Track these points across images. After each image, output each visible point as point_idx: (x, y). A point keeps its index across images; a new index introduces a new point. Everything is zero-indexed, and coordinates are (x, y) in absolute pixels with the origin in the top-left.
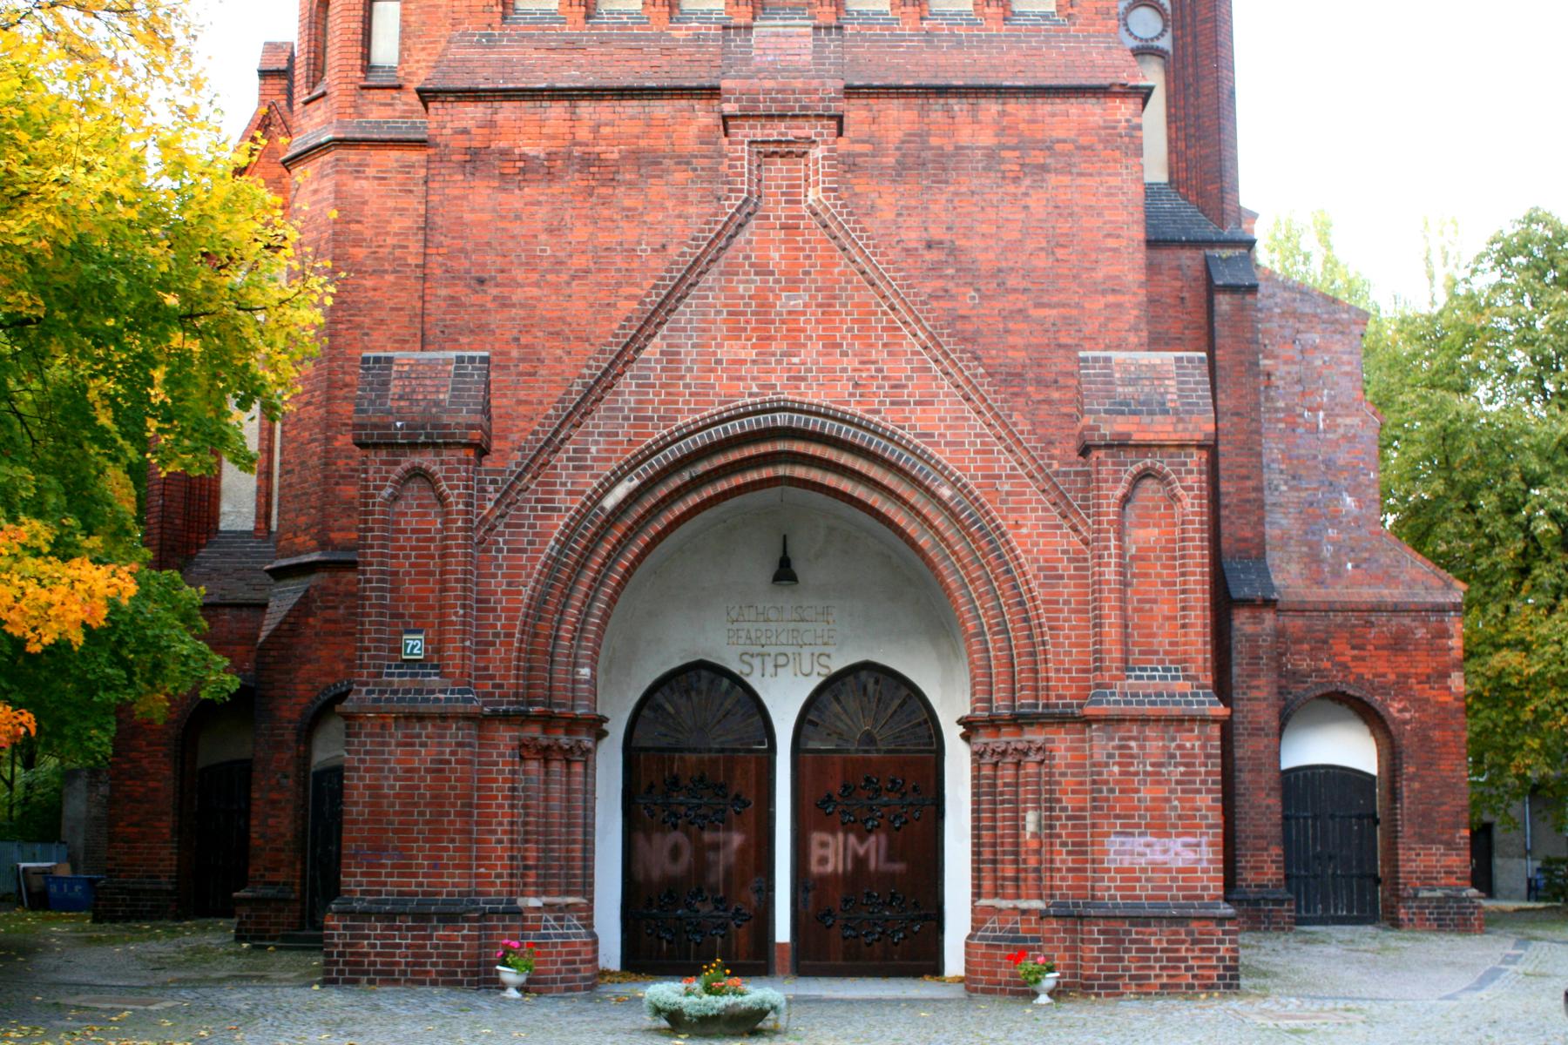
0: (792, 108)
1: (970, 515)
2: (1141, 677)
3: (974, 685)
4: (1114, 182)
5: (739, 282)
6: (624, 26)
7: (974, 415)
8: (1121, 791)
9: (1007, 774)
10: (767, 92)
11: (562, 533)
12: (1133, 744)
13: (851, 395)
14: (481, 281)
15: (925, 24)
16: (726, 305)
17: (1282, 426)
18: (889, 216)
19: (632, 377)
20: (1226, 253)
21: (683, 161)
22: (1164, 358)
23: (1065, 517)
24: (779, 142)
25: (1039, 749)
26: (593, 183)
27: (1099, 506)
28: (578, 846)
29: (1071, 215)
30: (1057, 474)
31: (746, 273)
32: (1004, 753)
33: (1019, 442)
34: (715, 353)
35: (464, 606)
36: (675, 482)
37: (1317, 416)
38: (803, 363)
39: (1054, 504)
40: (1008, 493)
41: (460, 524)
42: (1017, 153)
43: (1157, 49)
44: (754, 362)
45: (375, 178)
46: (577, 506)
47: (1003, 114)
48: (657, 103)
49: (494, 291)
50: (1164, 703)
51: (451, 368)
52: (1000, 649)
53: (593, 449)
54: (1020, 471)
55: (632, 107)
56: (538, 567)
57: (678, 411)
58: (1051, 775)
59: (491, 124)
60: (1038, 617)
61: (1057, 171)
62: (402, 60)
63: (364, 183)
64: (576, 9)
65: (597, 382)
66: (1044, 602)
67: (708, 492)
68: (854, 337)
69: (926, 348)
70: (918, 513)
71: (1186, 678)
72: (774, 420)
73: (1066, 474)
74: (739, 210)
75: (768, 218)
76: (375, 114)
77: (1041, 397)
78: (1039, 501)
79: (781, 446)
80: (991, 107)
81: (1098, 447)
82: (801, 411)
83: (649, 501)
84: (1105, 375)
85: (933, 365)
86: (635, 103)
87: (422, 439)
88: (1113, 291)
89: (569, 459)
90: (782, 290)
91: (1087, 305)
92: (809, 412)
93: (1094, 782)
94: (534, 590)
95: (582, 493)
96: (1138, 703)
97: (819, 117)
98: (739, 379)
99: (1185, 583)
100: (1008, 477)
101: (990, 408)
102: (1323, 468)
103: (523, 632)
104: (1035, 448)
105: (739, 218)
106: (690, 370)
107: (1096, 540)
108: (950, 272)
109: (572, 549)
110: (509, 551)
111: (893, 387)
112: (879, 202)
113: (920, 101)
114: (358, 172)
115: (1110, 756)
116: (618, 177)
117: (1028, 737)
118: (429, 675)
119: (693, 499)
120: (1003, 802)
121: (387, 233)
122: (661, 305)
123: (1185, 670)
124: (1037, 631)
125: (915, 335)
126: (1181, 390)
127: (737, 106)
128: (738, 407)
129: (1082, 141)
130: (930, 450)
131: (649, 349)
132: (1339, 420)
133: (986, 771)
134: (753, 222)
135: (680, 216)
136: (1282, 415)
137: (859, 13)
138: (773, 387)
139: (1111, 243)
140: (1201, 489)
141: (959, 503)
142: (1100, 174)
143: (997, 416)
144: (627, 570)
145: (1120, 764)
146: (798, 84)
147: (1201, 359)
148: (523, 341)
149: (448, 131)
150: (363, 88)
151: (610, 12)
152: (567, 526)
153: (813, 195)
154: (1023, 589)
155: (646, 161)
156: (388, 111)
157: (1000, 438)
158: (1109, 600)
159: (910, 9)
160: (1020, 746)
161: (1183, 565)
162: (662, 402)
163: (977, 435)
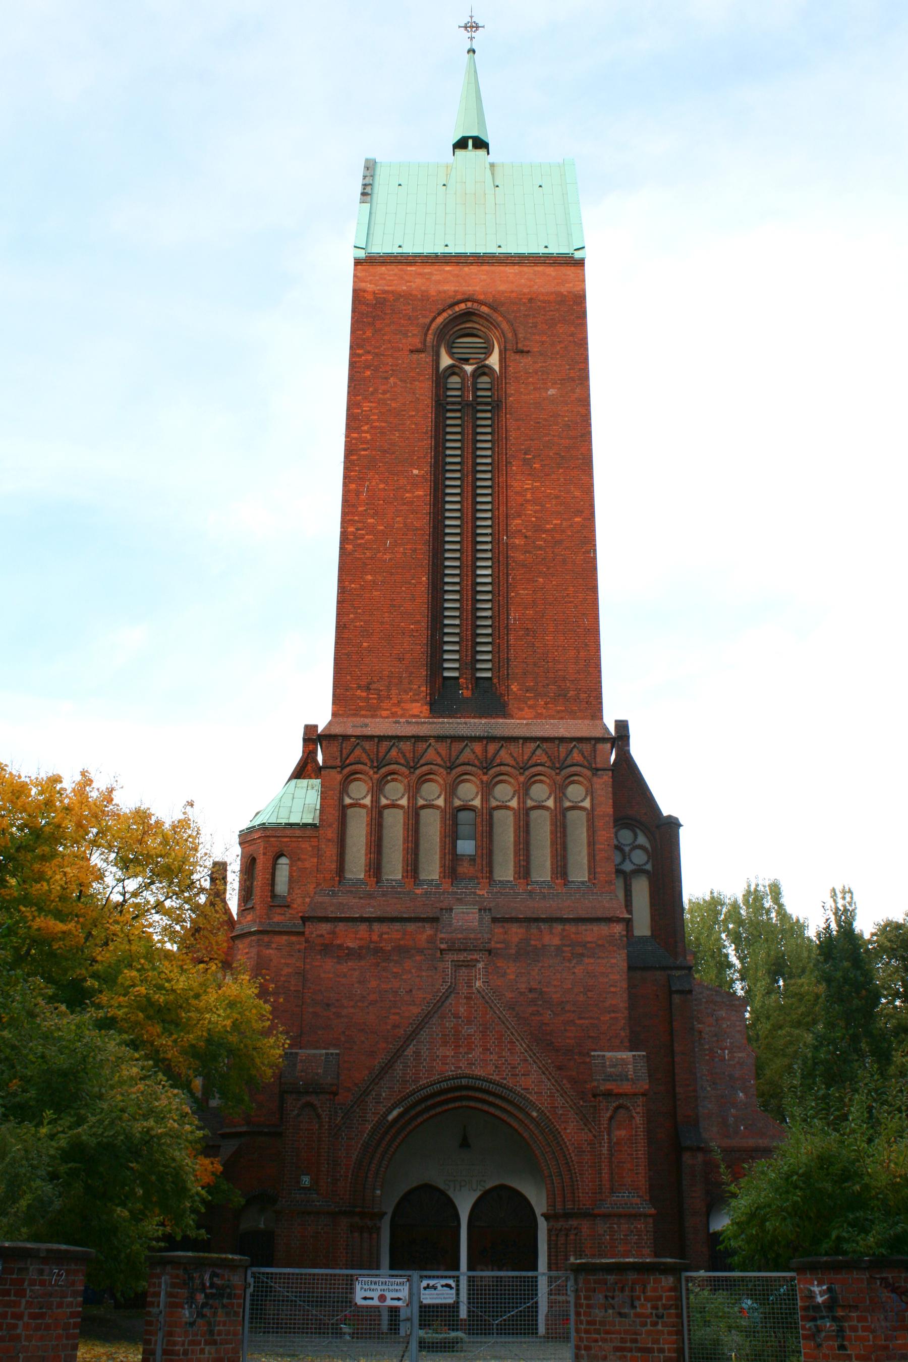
0: (470, 946)
1: (545, 1124)
2: (619, 1196)
3: (548, 1199)
4: (614, 961)
5: (447, 1021)
6: (393, 887)
7: (546, 1080)
8: (611, 1247)
9: (562, 1240)
10: (460, 939)
11: (370, 1131)
12: (615, 1226)
13: (494, 1071)
14: (328, 1005)
15: (529, 887)
16: (441, 1032)
17: (707, 1057)
18: (513, 977)
19: (401, 1063)
20: (678, 973)
21: (421, 951)
22: (627, 1055)
23: (586, 1125)
24: (464, 961)
25: (575, 1228)
26: (379, 961)
27: (600, 1121)
28: (553, 1261)
29: (594, 976)
30: (582, 1106)
31: (450, 1018)
32: (561, 1230)
33: (566, 1093)
34: (436, 1053)
35: (328, 1164)
36: (419, 1108)
37: (724, 1053)
38: (474, 1057)
39: (581, 1119)
40: (561, 1115)
41: (326, 1127)
42: (570, 948)
43: (645, 870)
44: (452, 1057)
45: (276, 949)
46: (376, 1119)
47: (563, 930)
48: (408, 924)
49: (334, 1010)
50: (629, 1208)
51: (323, 1058)
52: (559, 1183)
53: (384, 1094)
54: (566, 1105)
55: (397, 926)
56: (359, 1146)
57: (420, 1078)
58: (580, 1240)
59: (333, 933)
60: (575, 1169)
61: (589, 957)
62: (289, 893)
63: (271, 951)
64: (372, 879)
65: (386, 1064)
66: (577, 1162)
67: (433, 1112)
68: (495, 1046)
69: (526, 1051)
70: (523, 1122)
71: (638, 1196)
72: (461, 1082)
73: (587, 1106)
74: (446, 990)
75: (459, 993)
76: (277, 918)
77: (581, 1061)
78: (574, 1118)
79: (464, 1093)
80: (559, 927)
81: (599, 1095)
82: (473, 1078)
83: (407, 1117)
84: (603, 1063)
85: (529, 1058)
86: (398, 924)
87: (311, 1090)
88: (613, 1011)
89: (373, 1099)
90: (465, 1025)
91: (602, 1018)
92: (477, 1079)
93: (599, 1243)
94: (357, 1156)
95: (379, 1113)
96: (617, 1208)
97: (481, 950)
98: (447, 1064)
99: (637, 1154)
100: (562, 1107)
101: (553, 1077)
102: (728, 1079)
103: (352, 1175)
104: (572, 1095)
105: (446, 994)
106: (425, 1060)
107: (599, 1136)
108: (540, 1003)
109: (374, 1139)
110: (347, 1139)
111: (511, 1068)
112: (508, 971)
113: (526, 924)
114: (268, 946)
115: (605, 1231)
116: (391, 958)
117: (570, 1223)
118: (312, 1194)
119: (426, 1116)
120: (560, 1252)
121: (281, 975)
122: (414, 1031)
123: (637, 1193)
124: (574, 1175)
125: (521, 1045)
126: (634, 1070)
127: (446, 945)
128: (445, 1077)
129: (600, 942)
130: (528, 1095)
131: (408, 1050)
132: (735, 1054)
133: (553, 1238)
134: (453, 995)
135: (418, 976)
136: (707, 1052)
137: (500, 881)
138: (461, 1067)
139: (612, 989)
140: (643, 1113)
141: (540, 1119)
142: (607, 957)
143: (556, 1081)
144: (397, 1147)
145: (610, 1235)
146: (472, 936)
147: (643, 1055)
148: (346, 1033)
149: (314, 935)
150: (271, 906)
151: (387, 880)
152: (372, 1128)
153: (478, 984)
154: (568, 1157)
155: (402, 951)
156: (283, 917)
157: (558, 1091)
158: (604, 1162)
159: (522, 881)
160: (567, 1227)
161: (636, 1147)
162: (413, 1074)
163: (548, 1089)
